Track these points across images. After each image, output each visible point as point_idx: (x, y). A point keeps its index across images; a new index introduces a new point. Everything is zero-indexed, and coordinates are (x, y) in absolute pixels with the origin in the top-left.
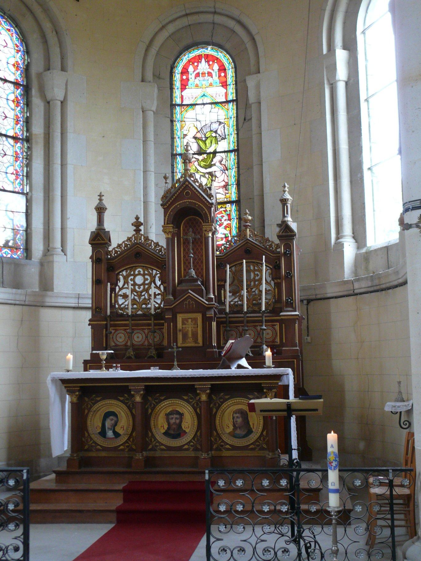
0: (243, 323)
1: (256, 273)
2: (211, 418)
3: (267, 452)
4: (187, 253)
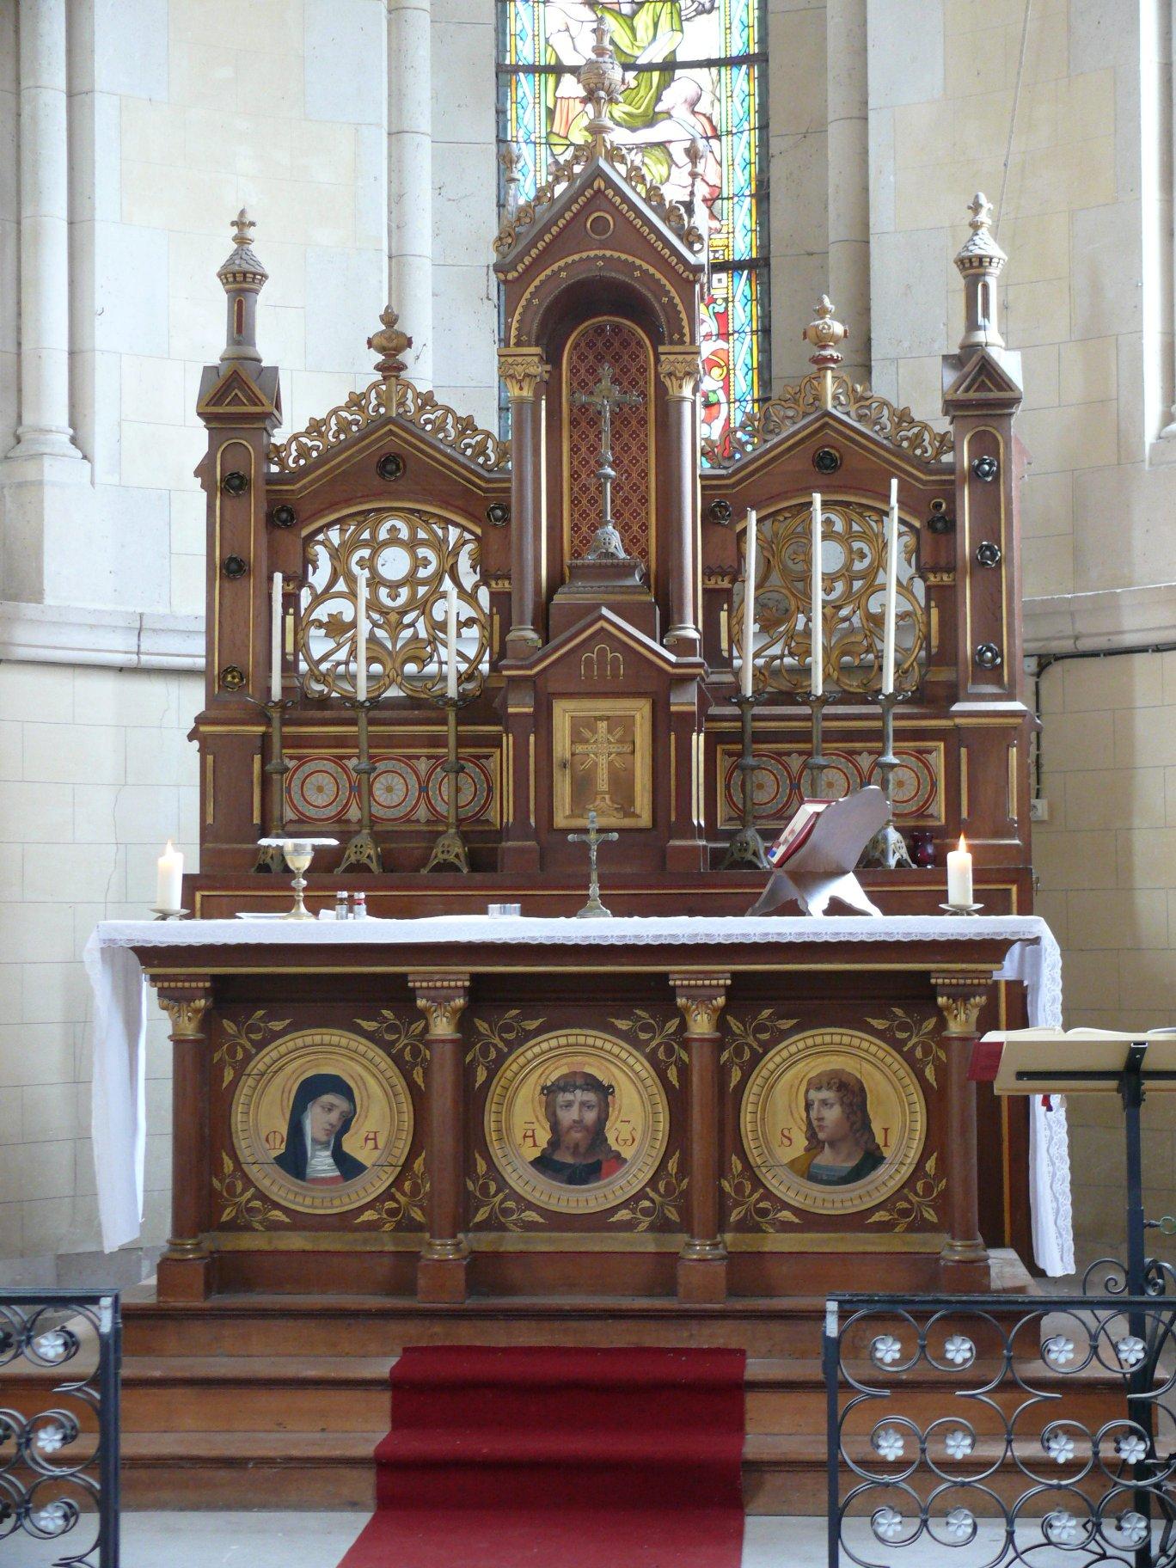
0: (809, 741)
1: (856, 545)
2: (727, 1102)
3: (945, 1238)
4: (587, 460)
